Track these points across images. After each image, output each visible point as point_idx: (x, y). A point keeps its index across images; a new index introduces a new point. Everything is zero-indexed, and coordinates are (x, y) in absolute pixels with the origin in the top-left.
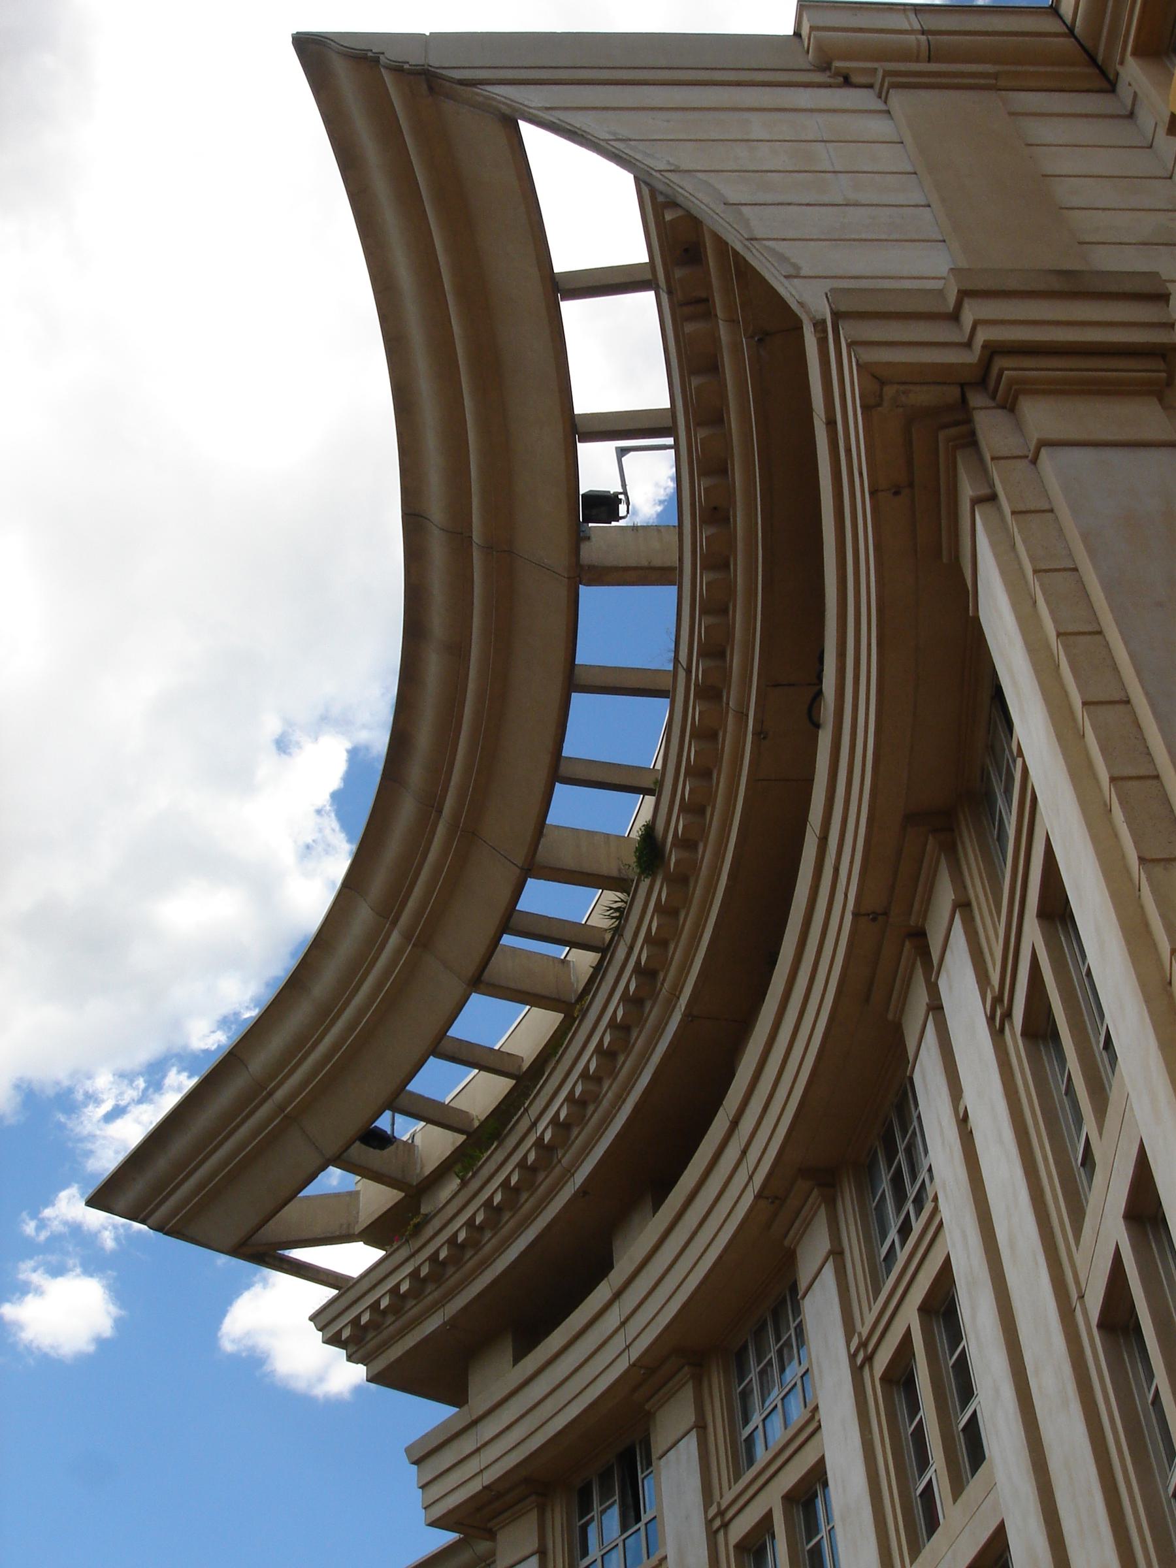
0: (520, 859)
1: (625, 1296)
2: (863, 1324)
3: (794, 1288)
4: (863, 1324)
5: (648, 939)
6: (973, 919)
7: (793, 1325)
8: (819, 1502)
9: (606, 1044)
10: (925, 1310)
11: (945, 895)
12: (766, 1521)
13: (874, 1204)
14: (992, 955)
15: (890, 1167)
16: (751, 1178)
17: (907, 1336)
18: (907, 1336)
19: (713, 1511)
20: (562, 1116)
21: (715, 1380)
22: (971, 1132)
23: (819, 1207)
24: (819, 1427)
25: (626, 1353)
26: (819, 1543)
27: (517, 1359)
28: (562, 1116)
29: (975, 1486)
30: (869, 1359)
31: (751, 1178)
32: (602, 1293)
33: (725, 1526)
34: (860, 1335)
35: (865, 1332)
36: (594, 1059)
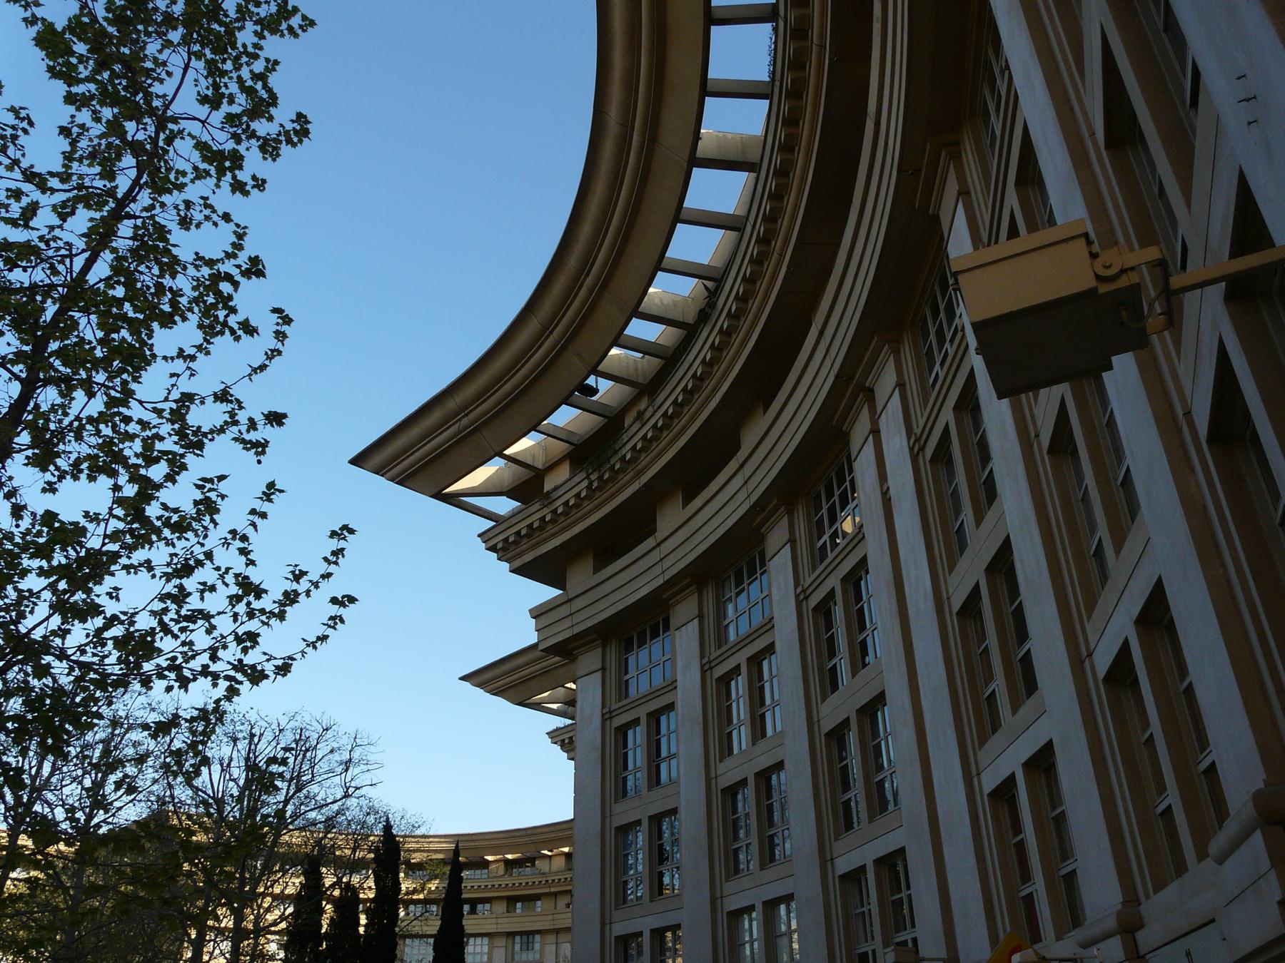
0: (686, 154)
1: (746, 467)
2: (918, 427)
3: (849, 457)
4: (918, 427)
5: (751, 261)
6: (900, 358)
7: (848, 479)
8: (863, 583)
9: (716, 344)
10: (957, 408)
11: (952, 187)
12: (832, 593)
13: (925, 352)
14: (984, 226)
15: (935, 323)
16: (832, 365)
17: (946, 428)
18: (946, 428)
19: (799, 590)
20: (708, 358)
21: (801, 510)
22: (890, 499)
23: (864, 404)
24: (864, 537)
25: (748, 500)
26: (862, 606)
27: (684, 506)
28: (708, 358)
29: (991, 516)
30: (922, 449)
31: (832, 365)
32: (733, 465)
33: (806, 598)
34: (916, 434)
35: (918, 431)
36: (718, 337)
